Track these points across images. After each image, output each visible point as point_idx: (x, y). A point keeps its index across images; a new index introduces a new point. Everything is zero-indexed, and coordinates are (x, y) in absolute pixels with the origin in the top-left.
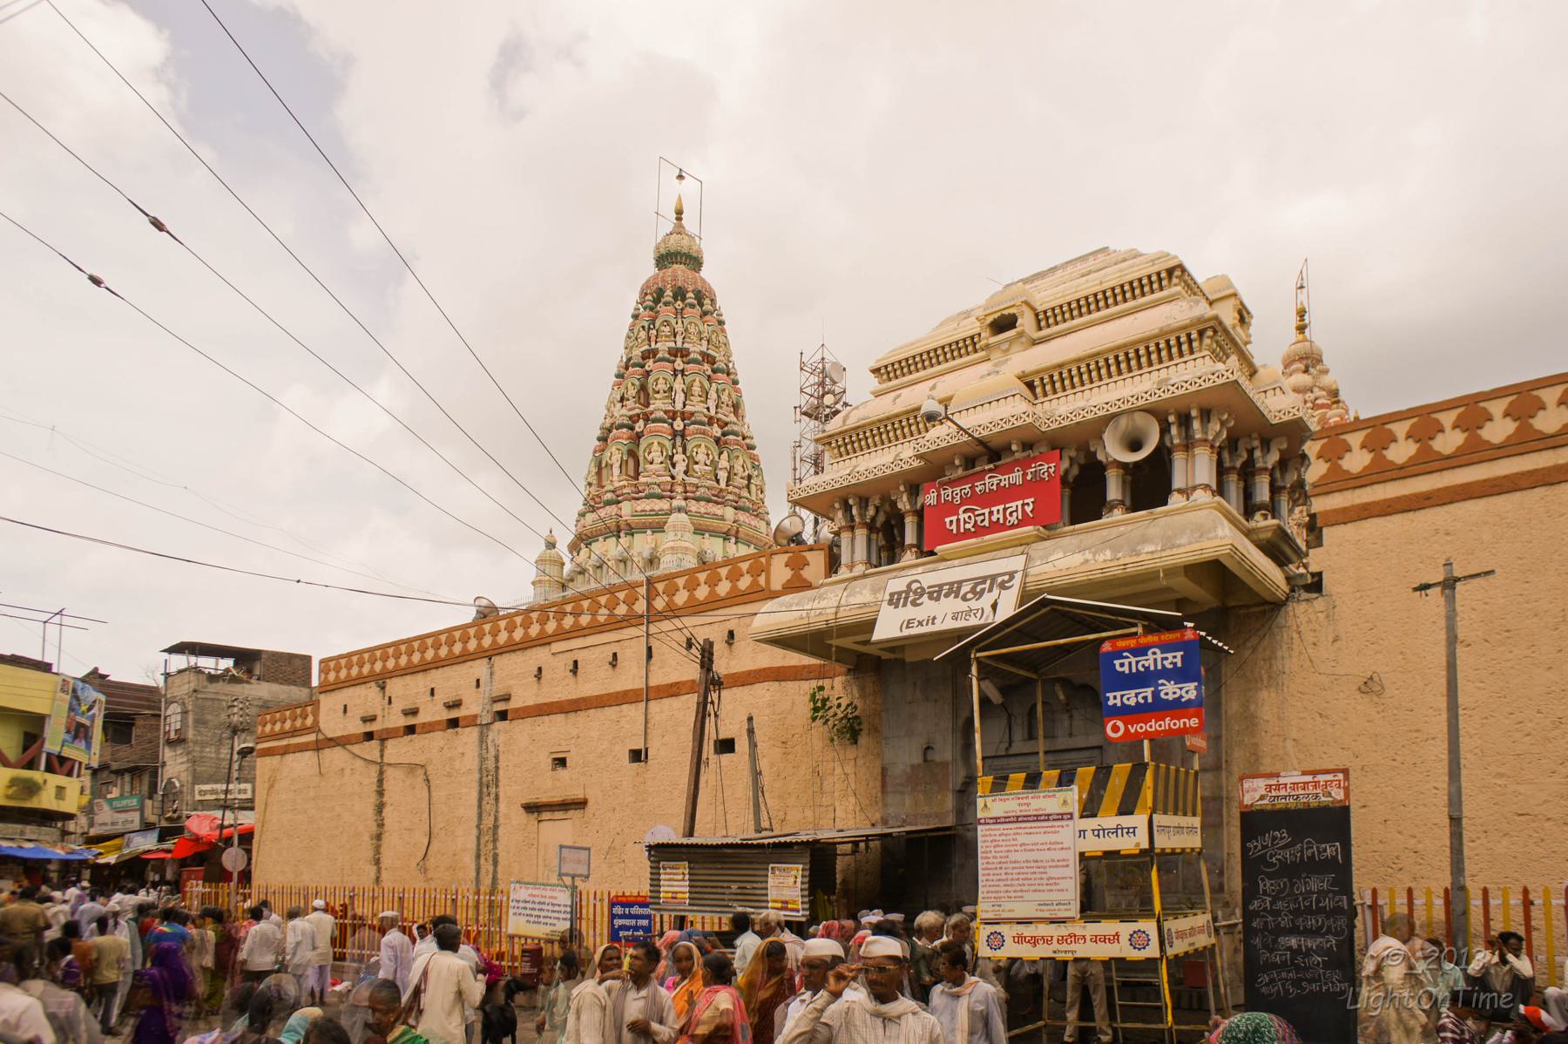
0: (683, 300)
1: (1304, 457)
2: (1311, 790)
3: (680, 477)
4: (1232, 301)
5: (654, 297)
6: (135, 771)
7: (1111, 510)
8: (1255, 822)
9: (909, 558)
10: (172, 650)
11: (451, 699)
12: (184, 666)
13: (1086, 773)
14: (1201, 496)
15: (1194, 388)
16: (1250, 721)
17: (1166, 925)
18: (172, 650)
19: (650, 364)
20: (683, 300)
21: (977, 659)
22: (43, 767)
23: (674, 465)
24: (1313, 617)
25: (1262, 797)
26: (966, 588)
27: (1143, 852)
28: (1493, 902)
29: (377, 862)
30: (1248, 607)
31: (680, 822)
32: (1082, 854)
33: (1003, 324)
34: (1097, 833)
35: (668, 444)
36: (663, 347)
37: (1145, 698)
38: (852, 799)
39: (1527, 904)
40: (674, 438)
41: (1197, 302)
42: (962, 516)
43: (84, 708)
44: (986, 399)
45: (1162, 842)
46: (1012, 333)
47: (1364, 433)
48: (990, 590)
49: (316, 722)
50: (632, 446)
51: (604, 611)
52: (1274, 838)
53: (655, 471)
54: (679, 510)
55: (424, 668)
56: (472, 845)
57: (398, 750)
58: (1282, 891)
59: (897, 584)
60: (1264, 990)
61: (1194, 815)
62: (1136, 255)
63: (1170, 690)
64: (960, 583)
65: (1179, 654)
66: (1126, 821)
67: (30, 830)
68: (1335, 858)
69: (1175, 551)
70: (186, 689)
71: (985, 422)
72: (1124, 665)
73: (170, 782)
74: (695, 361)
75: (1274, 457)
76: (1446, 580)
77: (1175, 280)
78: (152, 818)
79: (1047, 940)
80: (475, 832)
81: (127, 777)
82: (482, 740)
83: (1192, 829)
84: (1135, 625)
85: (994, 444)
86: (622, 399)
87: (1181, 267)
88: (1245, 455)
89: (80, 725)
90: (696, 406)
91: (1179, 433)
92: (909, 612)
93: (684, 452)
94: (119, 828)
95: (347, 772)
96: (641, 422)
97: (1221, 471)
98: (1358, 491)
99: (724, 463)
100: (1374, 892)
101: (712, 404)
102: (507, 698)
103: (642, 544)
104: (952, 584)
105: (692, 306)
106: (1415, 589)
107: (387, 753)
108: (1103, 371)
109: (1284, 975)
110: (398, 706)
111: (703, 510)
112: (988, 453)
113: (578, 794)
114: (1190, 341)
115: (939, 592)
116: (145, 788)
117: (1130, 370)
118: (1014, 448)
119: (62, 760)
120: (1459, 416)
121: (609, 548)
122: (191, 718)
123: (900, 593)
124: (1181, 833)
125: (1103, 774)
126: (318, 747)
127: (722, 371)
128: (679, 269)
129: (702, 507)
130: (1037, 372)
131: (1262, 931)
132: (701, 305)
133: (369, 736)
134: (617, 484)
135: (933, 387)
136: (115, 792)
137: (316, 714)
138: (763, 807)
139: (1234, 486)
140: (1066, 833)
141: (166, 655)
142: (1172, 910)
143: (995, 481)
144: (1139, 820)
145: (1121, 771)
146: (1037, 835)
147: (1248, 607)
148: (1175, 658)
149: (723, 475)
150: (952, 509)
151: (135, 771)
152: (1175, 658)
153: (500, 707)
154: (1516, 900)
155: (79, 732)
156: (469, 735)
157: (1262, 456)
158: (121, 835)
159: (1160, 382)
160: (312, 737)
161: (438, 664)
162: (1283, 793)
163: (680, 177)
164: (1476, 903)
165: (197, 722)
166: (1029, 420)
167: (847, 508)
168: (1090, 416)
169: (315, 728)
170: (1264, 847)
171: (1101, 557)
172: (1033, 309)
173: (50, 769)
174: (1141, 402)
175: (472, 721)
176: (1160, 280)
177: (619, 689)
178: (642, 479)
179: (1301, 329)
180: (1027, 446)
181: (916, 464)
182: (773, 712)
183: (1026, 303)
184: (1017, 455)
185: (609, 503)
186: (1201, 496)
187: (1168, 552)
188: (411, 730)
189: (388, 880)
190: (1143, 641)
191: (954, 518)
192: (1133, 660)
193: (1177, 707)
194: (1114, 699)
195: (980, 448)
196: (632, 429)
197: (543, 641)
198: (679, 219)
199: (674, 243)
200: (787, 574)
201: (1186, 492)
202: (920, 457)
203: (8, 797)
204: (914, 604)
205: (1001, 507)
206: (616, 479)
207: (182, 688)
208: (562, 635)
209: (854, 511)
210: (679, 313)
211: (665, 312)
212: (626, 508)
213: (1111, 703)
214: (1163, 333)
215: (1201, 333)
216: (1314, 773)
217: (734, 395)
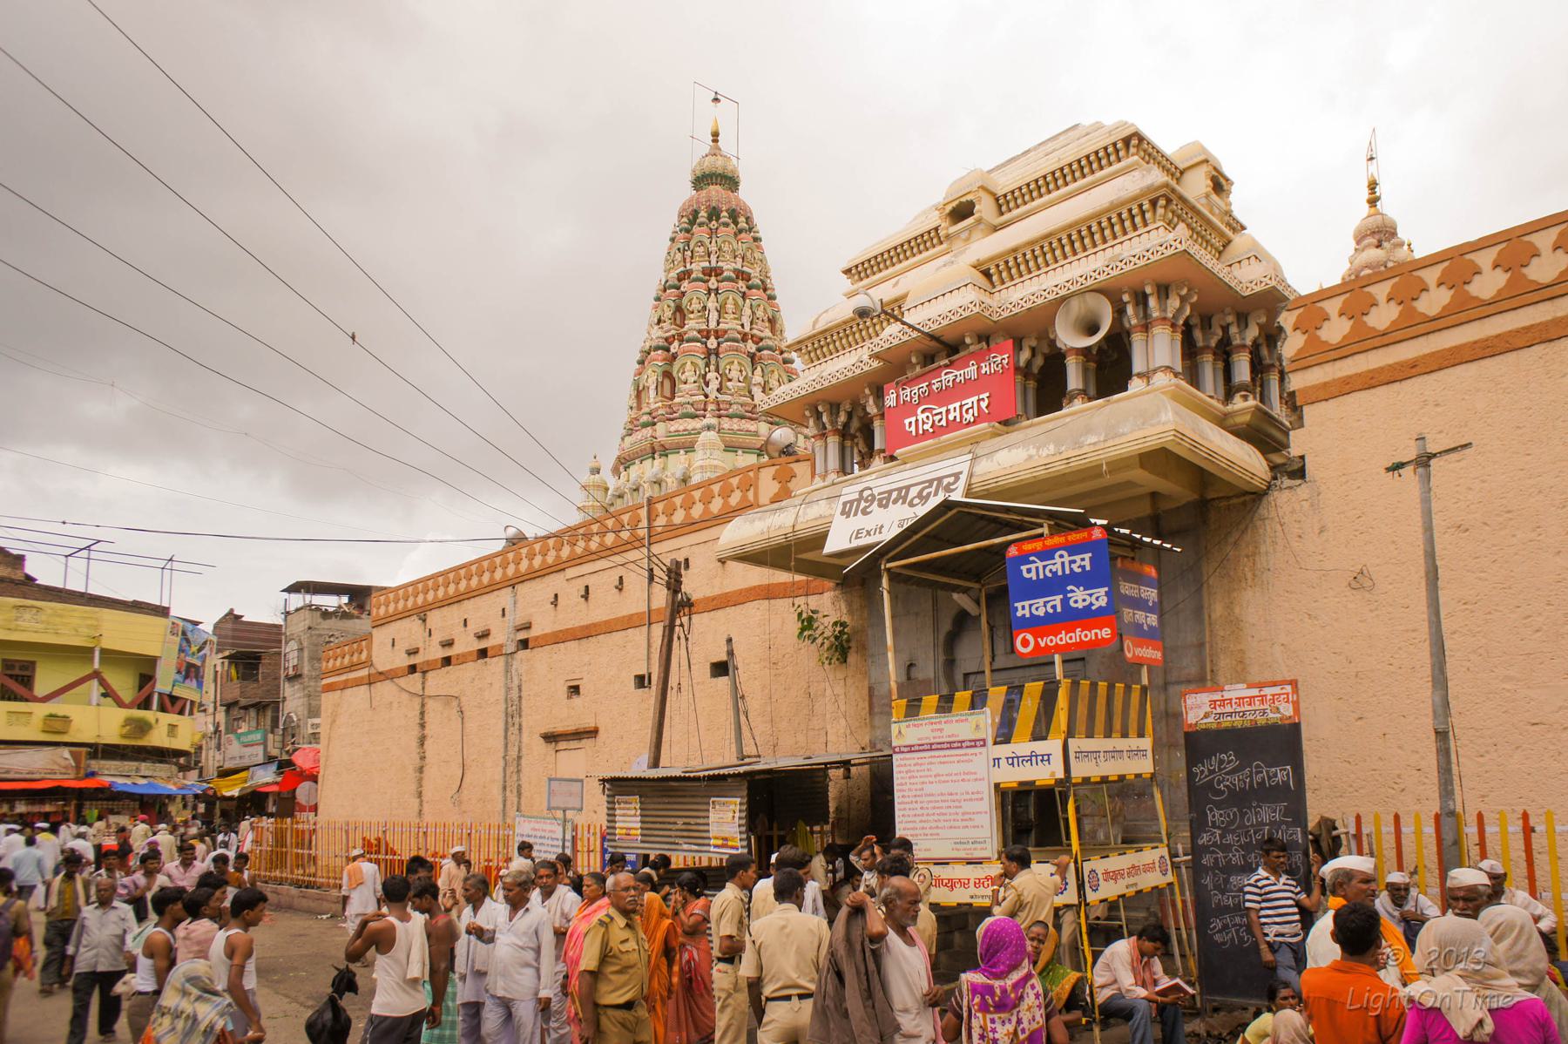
1: (1281, 329)
2: (1257, 706)
3: (713, 395)
4: (1204, 168)
5: (691, 218)
6: (260, 707)
7: (1071, 401)
8: (1199, 744)
9: (877, 463)
10: (295, 588)
11: (480, 630)
12: (300, 604)
13: (997, 694)
14: (1161, 379)
15: (1142, 263)
16: (1235, 624)
17: (1087, 867)
18: (295, 588)
19: (685, 285)
20: (718, 218)
21: (888, 570)
22: (155, 706)
23: (707, 384)
24: (1297, 507)
25: (1206, 716)
26: (914, 492)
27: (1059, 782)
28: (1489, 829)
29: (420, 795)
30: (1228, 498)
31: (645, 758)
32: (997, 786)
33: (962, 212)
34: (1013, 760)
35: (701, 364)
36: (697, 267)
37: (1054, 607)
38: (843, 722)
39: (1528, 831)
40: (708, 357)
41: (1149, 171)
42: (921, 417)
43: (194, 649)
44: (939, 293)
45: (1079, 770)
46: (970, 220)
47: (1343, 297)
48: (936, 494)
49: (369, 656)
50: (667, 368)
51: (596, 538)
52: (1221, 762)
53: (688, 392)
54: (709, 428)
55: (458, 599)
56: (499, 777)
57: (438, 681)
58: (1232, 822)
59: (850, 492)
60: (1217, 938)
61: (1141, 735)
62: (1098, 126)
63: (1079, 597)
64: (908, 488)
65: (1087, 556)
66: (1040, 747)
67: (146, 767)
68: (1286, 784)
69: (1117, 441)
70: (302, 626)
71: (934, 315)
72: (1032, 571)
73: (288, 716)
74: (729, 279)
75: (1253, 332)
76: (1419, 456)
77: (1132, 150)
78: (275, 752)
79: (964, 884)
80: (502, 763)
81: (253, 713)
82: (507, 670)
83: (1139, 752)
85: (947, 338)
86: (659, 321)
87: (1139, 137)
88: (1220, 333)
89: (190, 666)
90: (730, 324)
91: (1137, 315)
92: (858, 521)
93: (717, 370)
94: (246, 762)
95: (395, 705)
96: (676, 343)
97: (1190, 351)
98: (1338, 363)
99: (758, 378)
100: (1358, 819)
101: (746, 321)
102: (528, 627)
103: (676, 464)
104: (899, 490)
105: (726, 225)
106: (1388, 470)
107: (428, 684)
108: (1058, 253)
109: (1238, 920)
110: (438, 637)
111: (735, 427)
112: (942, 348)
113: (589, 723)
114: (1143, 213)
115: (888, 499)
116: (269, 722)
117: (1085, 249)
118: (968, 340)
119: (174, 699)
120: (1444, 272)
121: (645, 470)
122: (306, 654)
123: (851, 502)
124: (1129, 756)
125: (1016, 690)
127: (757, 287)
128: (715, 192)
129: (736, 424)
130: (992, 259)
131: (1212, 869)
132: (736, 223)
133: (413, 669)
135: (896, 284)
136: (244, 728)
137: (369, 649)
138: (745, 728)
139: (1209, 369)
140: (979, 761)
141: (286, 595)
142: (1094, 846)
143: (951, 377)
144: (1053, 746)
145: (1034, 689)
146: (950, 764)
147: (1228, 498)
148: (1084, 561)
150: (908, 408)
151: (260, 707)
152: (1084, 561)
153: (522, 635)
154: (1516, 827)
155: (191, 672)
156: (496, 665)
157: (1234, 332)
158: (247, 769)
159: (1111, 259)
160: (364, 673)
161: (470, 595)
162: (1228, 709)
163: (716, 100)
164: (1471, 830)
165: (311, 659)
166: (976, 310)
167: (818, 416)
168: (1040, 301)
169: (369, 663)
170: (1211, 772)
171: (1044, 452)
172: (993, 194)
173: (163, 709)
174: (1090, 282)
175: (499, 651)
176: (1117, 151)
177: (625, 613)
178: (677, 400)
179: (1373, 202)
180: (984, 337)
181: (876, 364)
182: (766, 632)
183: (983, 188)
184: (972, 348)
185: (645, 425)
186: (1161, 379)
187: (1110, 443)
188: (447, 661)
189: (428, 818)
190: (1049, 542)
191: (913, 419)
192: (1040, 564)
193: (1087, 617)
194: (1022, 609)
195: (934, 344)
196: (668, 350)
197: (558, 568)
198: (715, 141)
199: (710, 164)
200: (774, 487)
201: (1146, 376)
202: (876, 356)
203: (124, 736)
204: (865, 513)
205: (957, 405)
206: (652, 400)
207: (298, 626)
208: (576, 561)
209: (825, 419)
210: (712, 233)
211: (700, 233)
212: (661, 428)
213: (1019, 614)
214: (1113, 207)
215: (1154, 203)
216: (1261, 686)
217: (769, 310)
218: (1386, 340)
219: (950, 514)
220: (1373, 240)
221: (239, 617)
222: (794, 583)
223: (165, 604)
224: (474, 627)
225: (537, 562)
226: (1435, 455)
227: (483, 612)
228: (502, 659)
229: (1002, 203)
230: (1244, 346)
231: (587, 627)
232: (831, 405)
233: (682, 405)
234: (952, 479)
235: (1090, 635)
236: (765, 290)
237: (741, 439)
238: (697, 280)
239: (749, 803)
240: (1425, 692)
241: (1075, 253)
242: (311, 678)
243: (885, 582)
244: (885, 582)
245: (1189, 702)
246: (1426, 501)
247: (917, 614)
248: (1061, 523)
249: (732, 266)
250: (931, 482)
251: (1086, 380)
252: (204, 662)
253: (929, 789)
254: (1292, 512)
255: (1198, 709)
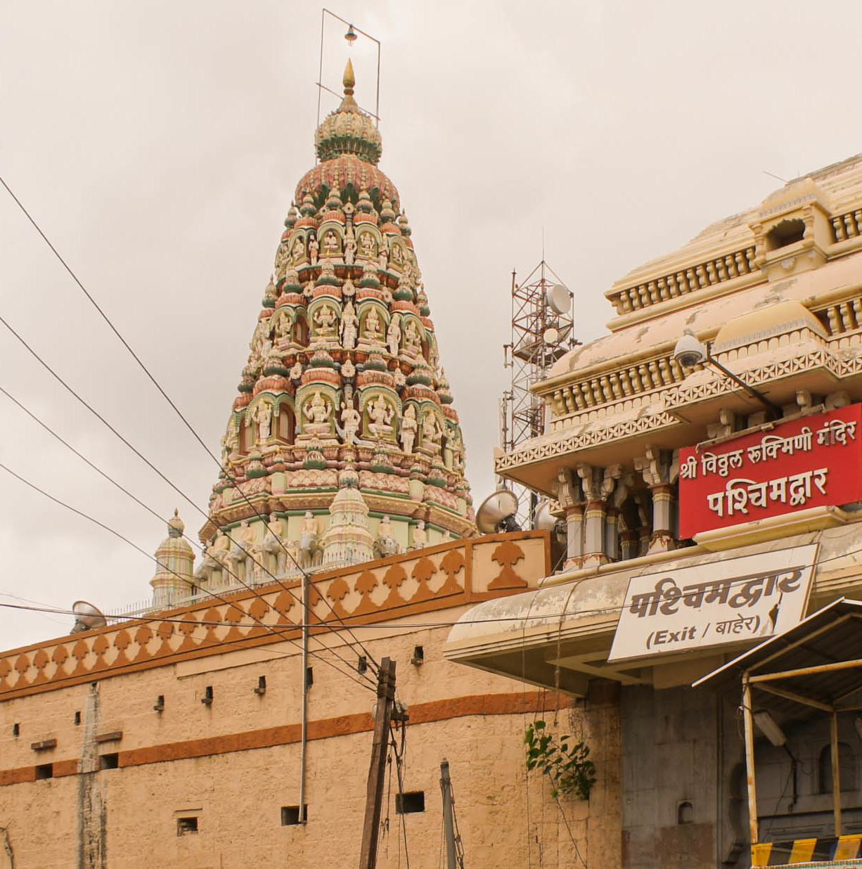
3: (350, 439)
5: (315, 197)
9: (658, 549)
11: (41, 739)
20: (355, 200)
21: (750, 685)
26: (735, 590)
35: (335, 396)
36: (327, 265)
42: (731, 493)
48: (769, 593)
50: (285, 399)
53: (315, 433)
54: (350, 484)
59: (643, 584)
64: (728, 583)
71: (761, 366)
82: (84, 794)
85: (773, 395)
86: (272, 335)
90: (370, 345)
92: (658, 622)
93: (356, 406)
101: (393, 341)
102: (117, 738)
103: (299, 531)
111: (381, 485)
112: (765, 407)
115: (700, 595)
118: (800, 400)
121: (254, 536)
123: (646, 597)
128: (349, 161)
129: (380, 481)
130: (831, 299)
132: (379, 208)
134: (265, 450)
143: (775, 445)
149: (408, 438)
150: (717, 483)
156: (66, 788)
163: (351, 36)
166: (820, 364)
167: (575, 482)
175: (70, 769)
180: (818, 398)
181: (668, 422)
183: (817, 206)
185: (255, 475)
191: (720, 495)
195: (755, 401)
196: (286, 375)
197: (166, 661)
198: (349, 92)
199: (343, 125)
200: (495, 570)
202: (673, 413)
204: (666, 611)
205: (783, 481)
206: (264, 443)
208: (192, 653)
210: (349, 219)
219: (840, 620)
222: (518, 696)
225: (132, 652)
232: (594, 469)
234: (790, 576)
236: (415, 302)
238: (327, 282)
247: (695, 741)
249: (374, 267)
250: (759, 578)
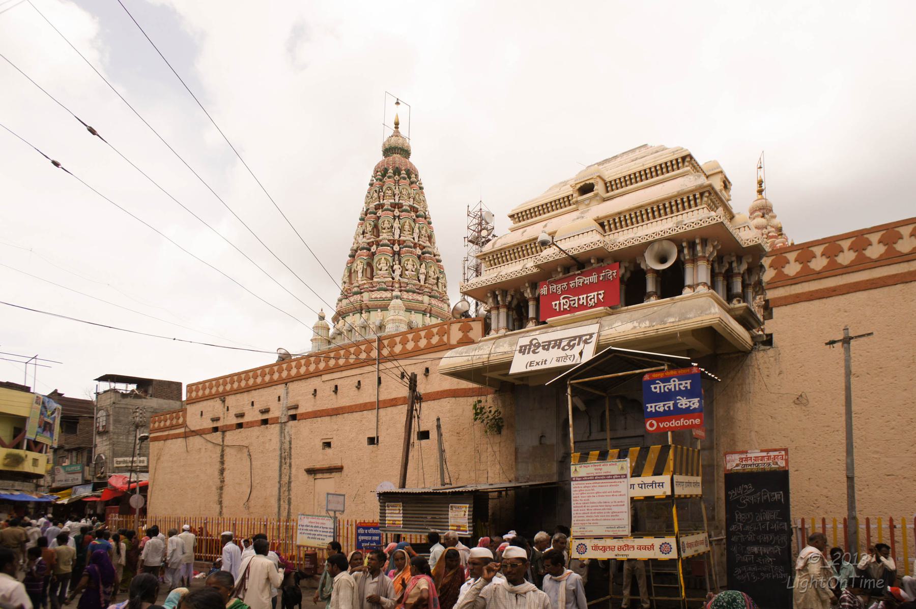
0: (399, 175)
1: (762, 266)
2: (766, 461)
3: (397, 278)
4: (720, 176)
5: (382, 173)
6: (79, 450)
7: (649, 298)
8: (733, 479)
9: (531, 325)
10: (101, 379)
11: (263, 408)
12: (108, 388)
13: (635, 450)
14: (702, 289)
16: (730, 421)
18: (101, 379)
19: (380, 212)
20: (399, 175)
22: (25, 447)
23: (394, 272)
25: (737, 465)
26: (564, 343)
29: (220, 503)
31: (397, 479)
32: (632, 498)
33: (586, 189)
34: (642, 485)
35: (390, 259)
36: (387, 202)
37: (669, 407)
40: (394, 256)
41: (699, 176)
42: (562, 301)
43: (49, 413)
44: (576, 233)
45: (679, 491)
46: (591, 194)
48: (579, 344)
49: (185, 421)
50: (370, 261)
52: (744, 489)
53: (383, 275)
54: (397, 297)
55: (248, 389)
57: (232, 437)
58: (749, 520)
59: (524, 341)
60: (738, 577)
63: (683, 402)
64: (561, 340)
65: (689, 382)
66: (658, 479)
67: (18, 485)
68: (780, 500)
69: (686, 322)
70: (108, 402)
71: (575, 246)
72: (657, 388)
73: (99, 456)
74: (406, 211)
75: (744, 267)
76: (844, 338)
77: (686, 164)
78: (89, 477)
79: (612, 548)
80: (278, 485)
81: (74, 454)
82: (282, 431)
83: (696, 484)
84: (663, 365)
86: (363, 233)
89: (47, 423)
90: (406, 237)
92: (531, 357)
94: (70, 483)
95: (203, 450)
96: (375, 247)
97: (713, 275)
98: (793, 287)
99: (423, 270)
100: (803, 520)
101: (416, 236)
102: (296, 407)
103: (375, 317)
104: (556, 341)
105: (404, 178)
106: (827, 344)
107: (226, 439)
109: (750, 569)
110: (233, 411)
111: (410, 298)
112: (576, 264)
113: (338, 463)
115: (549, 345)
116: (85, 459)
118: (592, 261)
119: (36, 443)
121: (355, 320)
123: (525, 346)
124: (690, 486)
126: (186, 436)
127: (422, 216)
128: (397, 157)
129: (410, 296)
132: (410, 178)
133: (216, 429)
135: (546, 226)
136: (67, 462)
137: (184, 417)
139: (721, 284)
143: (581, 281)
144: (665, 478)
145: (655, 449)
146: (606, 487)
147: (728, 354)
148: (687, 384)
151: (79, 450)
152: (687, 384)
153: (292, 412)
154: (885, 525)
155: (46, 427)
156: (274, 429)
157: (736, 265)
158: (71, 487)
159: (678, 223)
160: (182, 430)
161: (256, 387)
162: (749, 462)
163: (398, 103)
164: (862, 526)
166: (601, 245)
167: (495, 297)
168: (636, 243)
169: (184, 424)
170: (738, 494)
171: (643, 325)
172: (604, 180)
173: (29, 448)
174: (666, 235)
175: (276, 421)
177: (361, 402)
178: (375, 280)
179: (760, 192)
180: (600, 260)
181: (535, 270)
182: (451, 415)
183: (600, 177)
187: (683, 322)
190: (668, 374)
191: (557, 302)
192: (662, 385)
194: (651, 407)
195: (572, 261)
196: (369, 250)
197: (318, 374)
198: (397, 128)
200: (460, 335)
201: (693, 287)
204: (534, 352)
206: (360, 279)
208: (329, 370)
209: (499, 298)
210: (397, 183)
211: (389, 182)
212: (366, 296)
213: (649, 410)
214: (679, 194)
215: (702, 194)
216: (768, 451)
218: (819, 276)
219: (610, 356)
220: (760, 214)
221: (61, 395)
223: (27, 385)
224: (258, 406)
226: (852, 338)
227: (266, 398)
228: (278, 425)
229: (609, 186)
230: (739, 273)
231: (336, 409)
232: (503, 291)
233: (379, 283)
235: (689, 422)
237: (414, 304)
239: (474, 507)
240: (843, 456)
241: (654, 217)
242: (114, 433)
243: (569, 391)
244: (569, 391)
245: (728, 458)
246: (848, 360)
248: (676, 364)
251: (656, 288)
252: (54, 421)
253: (592, 499)
254: (765, 363)
255: (733, 463)
